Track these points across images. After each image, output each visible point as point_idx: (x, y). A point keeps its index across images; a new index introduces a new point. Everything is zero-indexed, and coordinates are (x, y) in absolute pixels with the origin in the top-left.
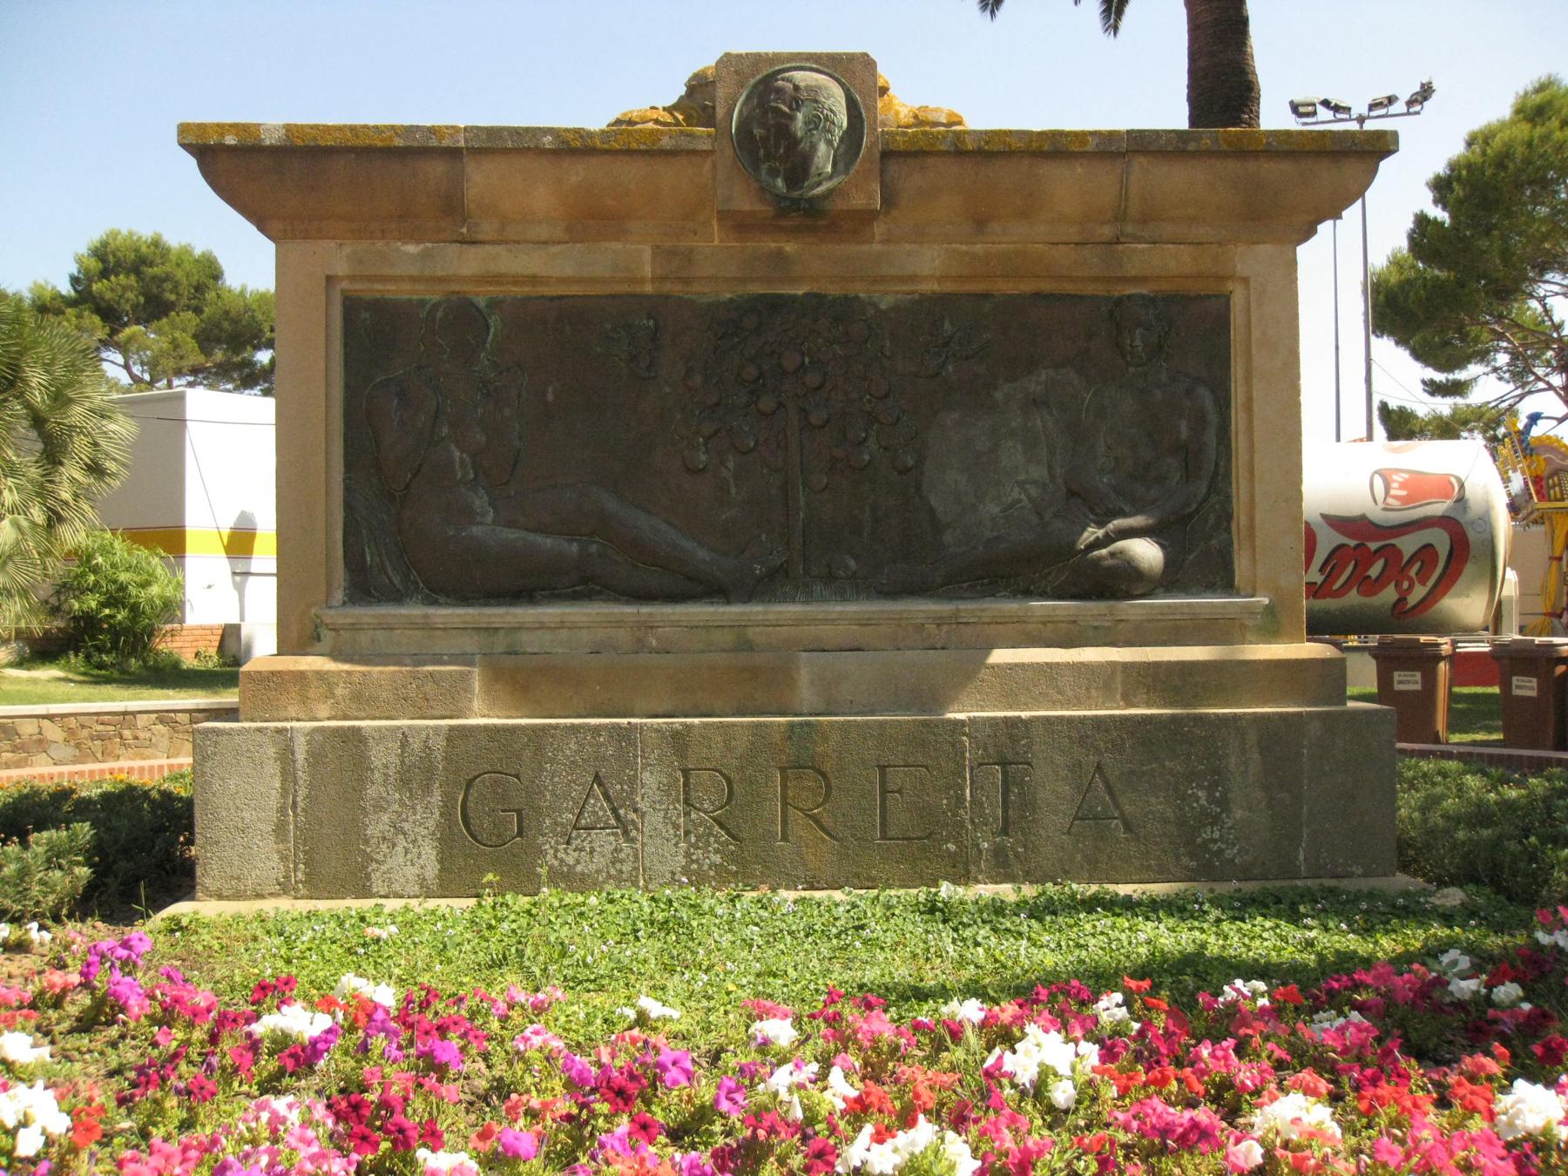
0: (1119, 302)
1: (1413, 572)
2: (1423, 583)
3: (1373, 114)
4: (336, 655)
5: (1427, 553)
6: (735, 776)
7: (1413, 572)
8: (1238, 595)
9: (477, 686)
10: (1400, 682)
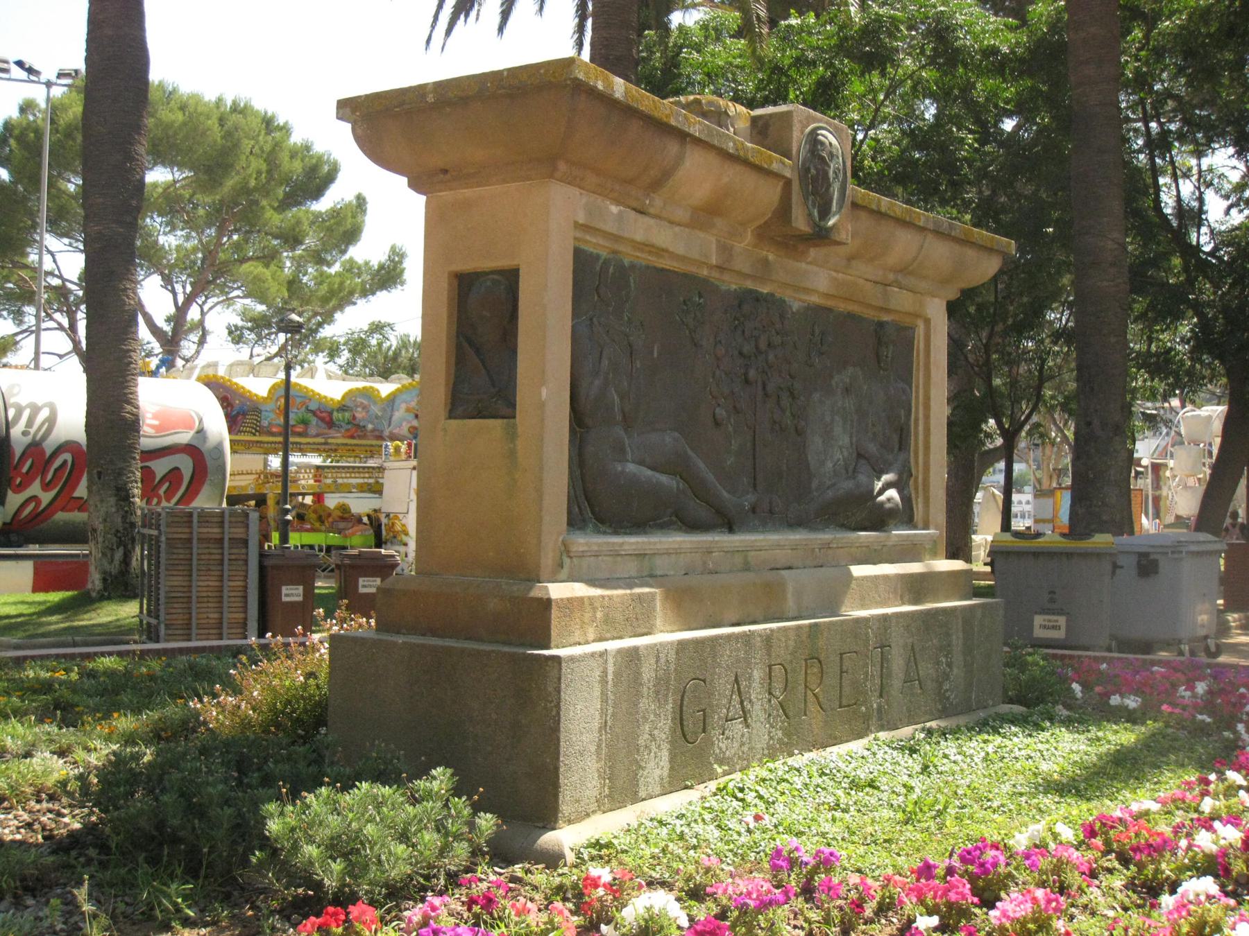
0: (881, 325)
1: (161, 492)
2: (168, 500)
3: (59, 81)
4: (592, 582)
5: (174, 474)
6: (789, 668)
7: (161, 492)
8: (915, 528)
9: (658, 604)
10: (364, 586)
